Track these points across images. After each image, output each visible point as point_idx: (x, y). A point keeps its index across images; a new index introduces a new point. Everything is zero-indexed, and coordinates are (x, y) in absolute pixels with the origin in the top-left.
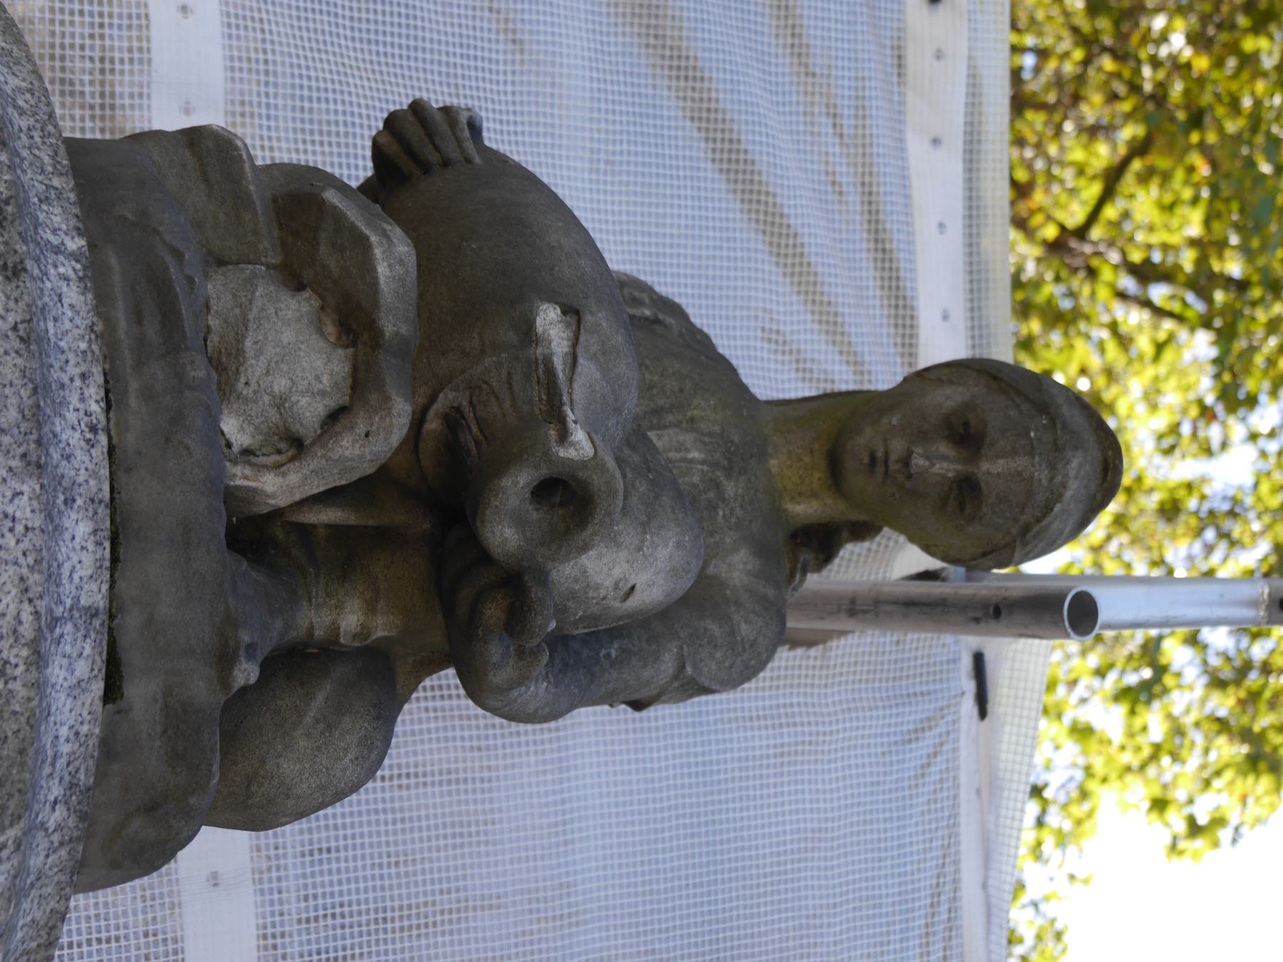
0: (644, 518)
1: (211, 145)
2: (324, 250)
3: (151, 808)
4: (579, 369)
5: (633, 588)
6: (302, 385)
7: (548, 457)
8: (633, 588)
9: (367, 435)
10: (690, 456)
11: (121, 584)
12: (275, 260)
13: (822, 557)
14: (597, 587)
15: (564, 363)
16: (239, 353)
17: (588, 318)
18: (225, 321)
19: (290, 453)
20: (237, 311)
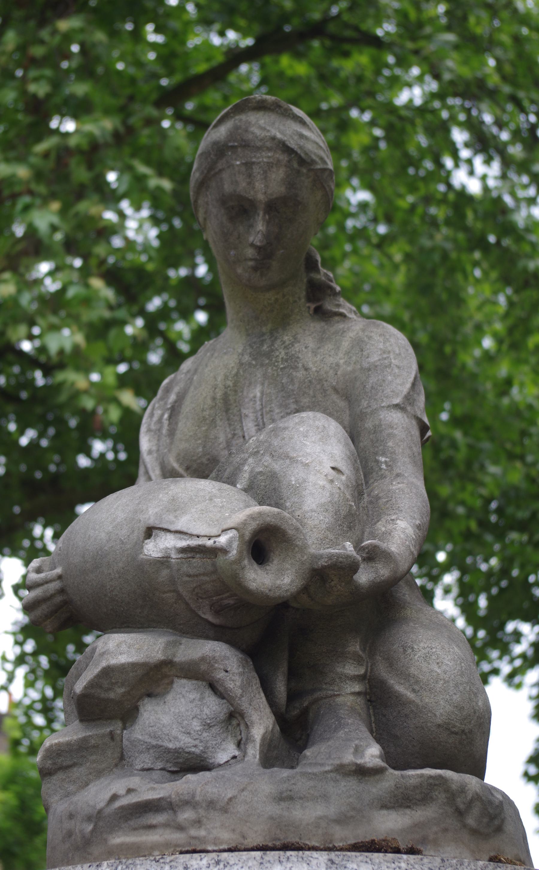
0: (288, 461)
1: (50, 762)
2: (112, 695)
3: (460, 814)
4: (185, 529)
5: (333, 468)
6: (197, 711)
7: (239, 561)
8: (333, 468)
9: (227, 671)
10: (258, 394)
11: (314, 843)
12: (120, 724)
13: (329, 292)
14: (332, 494)
15: (181, 539)
16: (177, 752)
17: (152, 522)
18: (157, 759)
19: (239, 718)
20: (151, 751)
